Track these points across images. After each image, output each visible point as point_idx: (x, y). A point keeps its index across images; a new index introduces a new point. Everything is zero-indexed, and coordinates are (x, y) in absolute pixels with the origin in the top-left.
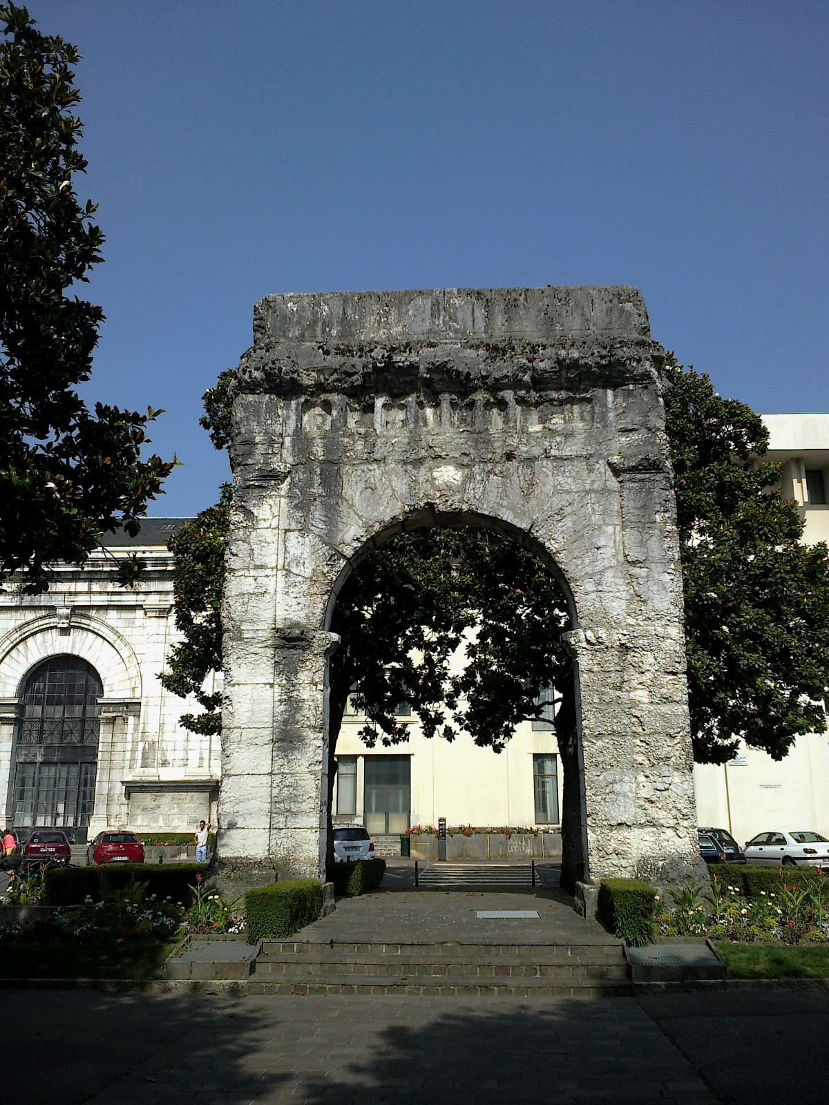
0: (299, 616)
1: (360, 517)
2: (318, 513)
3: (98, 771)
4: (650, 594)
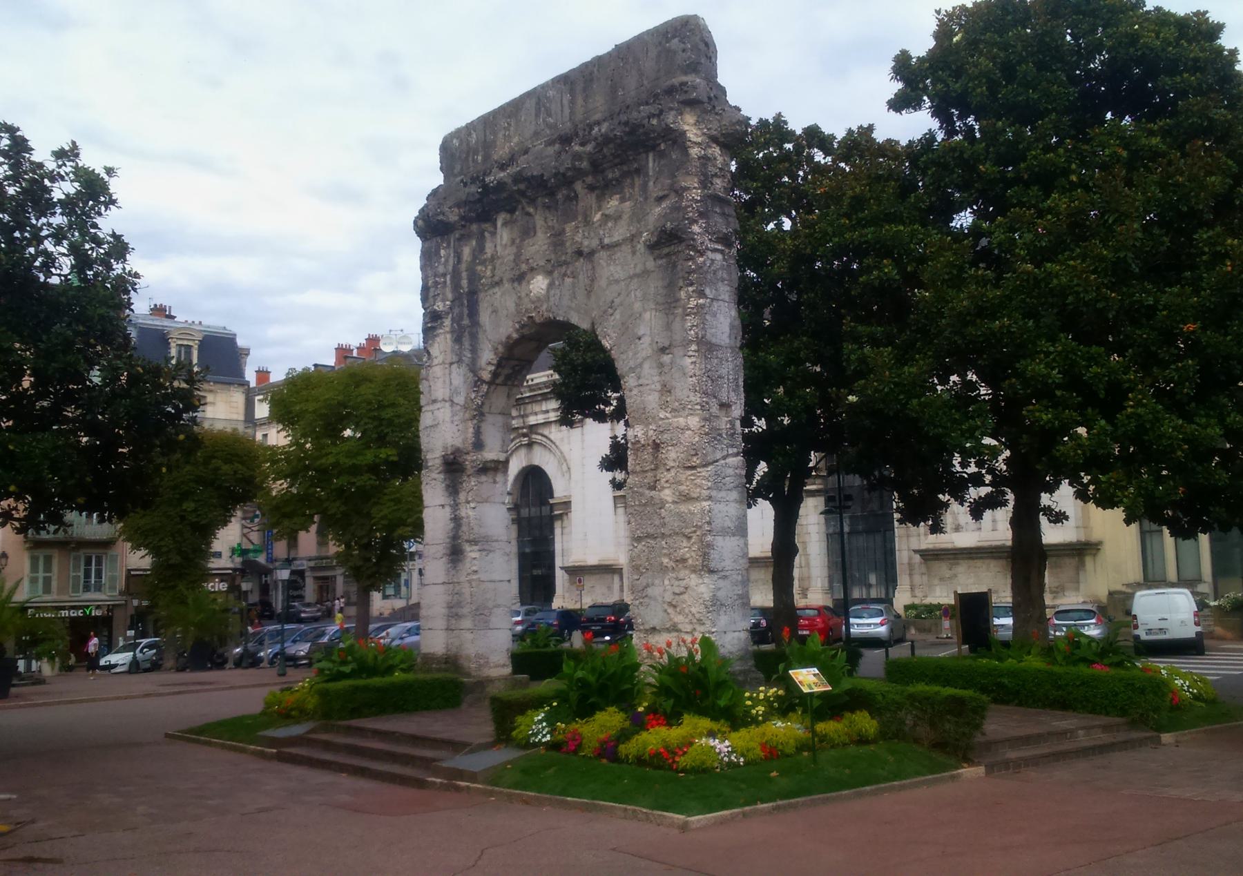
0: (458, 443)
1: (490, 341)
2: (467, 344)
3: (896, 539)
4: (674, 383)
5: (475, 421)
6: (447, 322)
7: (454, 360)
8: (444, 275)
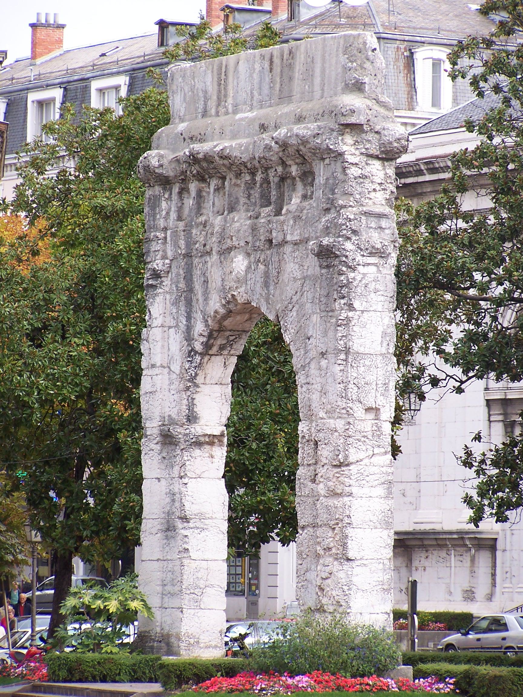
5: (189, 393)
6: (167, 282)
7: (172, 325)
8: (165, 229)
